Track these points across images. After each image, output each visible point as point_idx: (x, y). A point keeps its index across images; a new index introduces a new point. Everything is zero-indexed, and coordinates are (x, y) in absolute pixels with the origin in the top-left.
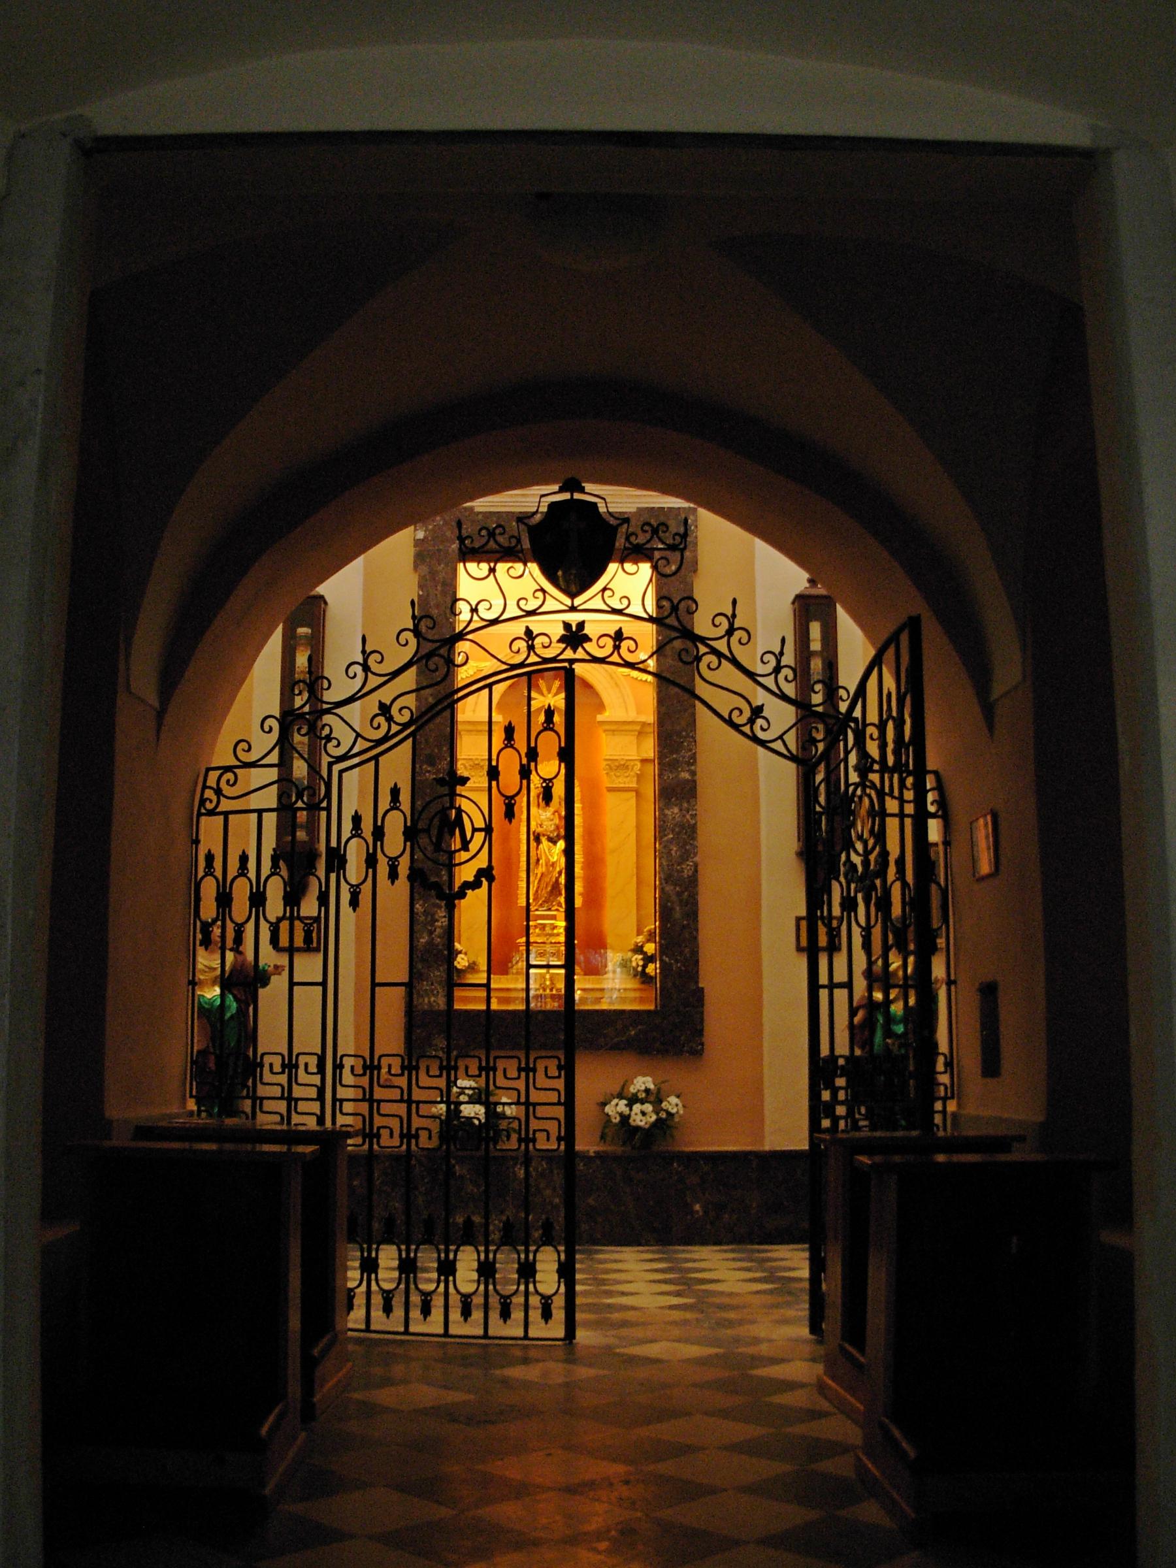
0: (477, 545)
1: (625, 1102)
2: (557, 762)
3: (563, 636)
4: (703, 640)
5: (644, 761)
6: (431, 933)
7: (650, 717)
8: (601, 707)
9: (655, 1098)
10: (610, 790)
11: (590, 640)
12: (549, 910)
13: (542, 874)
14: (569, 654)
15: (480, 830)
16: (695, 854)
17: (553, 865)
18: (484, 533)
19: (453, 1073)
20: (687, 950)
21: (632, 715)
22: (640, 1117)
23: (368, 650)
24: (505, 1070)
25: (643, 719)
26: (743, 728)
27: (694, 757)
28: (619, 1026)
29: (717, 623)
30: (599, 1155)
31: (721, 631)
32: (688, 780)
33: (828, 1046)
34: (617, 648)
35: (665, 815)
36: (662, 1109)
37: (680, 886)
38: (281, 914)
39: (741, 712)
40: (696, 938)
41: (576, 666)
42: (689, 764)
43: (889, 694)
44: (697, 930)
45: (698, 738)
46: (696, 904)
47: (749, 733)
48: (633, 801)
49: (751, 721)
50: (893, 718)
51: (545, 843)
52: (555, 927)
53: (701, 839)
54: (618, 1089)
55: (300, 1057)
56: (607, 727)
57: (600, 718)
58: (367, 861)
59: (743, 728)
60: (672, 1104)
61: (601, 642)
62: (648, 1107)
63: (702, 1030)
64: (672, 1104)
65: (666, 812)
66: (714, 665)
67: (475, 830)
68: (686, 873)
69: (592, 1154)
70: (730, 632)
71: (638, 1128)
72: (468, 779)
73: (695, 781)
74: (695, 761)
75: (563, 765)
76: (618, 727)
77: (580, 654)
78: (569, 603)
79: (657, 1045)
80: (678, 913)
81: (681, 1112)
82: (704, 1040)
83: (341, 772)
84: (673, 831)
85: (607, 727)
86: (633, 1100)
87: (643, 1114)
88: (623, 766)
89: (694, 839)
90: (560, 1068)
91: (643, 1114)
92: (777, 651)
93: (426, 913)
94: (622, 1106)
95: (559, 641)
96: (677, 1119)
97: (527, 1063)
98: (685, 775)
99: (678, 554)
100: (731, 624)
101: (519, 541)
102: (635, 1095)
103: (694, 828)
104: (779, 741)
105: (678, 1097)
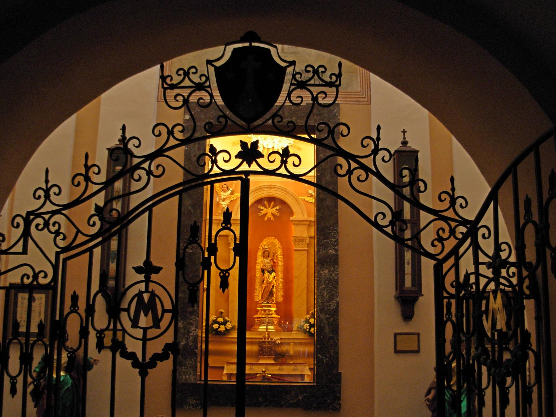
0: (174, 82)
3: (240, 153)
4: (354, 158)
5: (310, 238)
6: (187, 339)
7: (313, 218)
8: (292, 213)
10: (296, 250)
11: (262, 156)
12: (268, 303)
14: (245, 167)
15: (168, 311)
16: (337, 296)
17: (270, 283)
18: (181, 72)
20: (332, 351)
21: (306, 217)
23: (89, 164)
25: (310, 219)
27: (337, 241)
28: (293, 394)
29: (365, 144)
31: (368, 151)
32: (333, 254)
34: (284, 163)
35: (321, 274)
37: (329, 314)
38: (104, 326)
40: (337, 344)
41: (251, 178)
42: (334, 245)
43: (528, 202)
46: (337, 325)
48: (306, 255)
50: (534, 223)
51: (266, 274)
52: (271, 311)
53: (341, 288)
56: (295, 223)
57: (291, 218)
58: (80, 332)
61: (272, 158)
63: (340, 396)
65: (321, 272)
66: (363, 178)
67: (164, 311)
68: (333, 307)
70: (376, 151)
72: (160, 268)
73: (337, 255)
74: (338, 243)
75: (237, 258)
76: (299, 223)
77: (254, 167)
78: (246, 127)
79: (315, 405)
82: (341, 402)
83: (65, 260)
85: (295, 223)
88: (301, 240)
89: (337, 288)
93: (184, 328)
95: (236, 157)
98: (332, 252)
99: (334, 89)
100: (376, 146)
101: (208, 78)
103: (337, 282)
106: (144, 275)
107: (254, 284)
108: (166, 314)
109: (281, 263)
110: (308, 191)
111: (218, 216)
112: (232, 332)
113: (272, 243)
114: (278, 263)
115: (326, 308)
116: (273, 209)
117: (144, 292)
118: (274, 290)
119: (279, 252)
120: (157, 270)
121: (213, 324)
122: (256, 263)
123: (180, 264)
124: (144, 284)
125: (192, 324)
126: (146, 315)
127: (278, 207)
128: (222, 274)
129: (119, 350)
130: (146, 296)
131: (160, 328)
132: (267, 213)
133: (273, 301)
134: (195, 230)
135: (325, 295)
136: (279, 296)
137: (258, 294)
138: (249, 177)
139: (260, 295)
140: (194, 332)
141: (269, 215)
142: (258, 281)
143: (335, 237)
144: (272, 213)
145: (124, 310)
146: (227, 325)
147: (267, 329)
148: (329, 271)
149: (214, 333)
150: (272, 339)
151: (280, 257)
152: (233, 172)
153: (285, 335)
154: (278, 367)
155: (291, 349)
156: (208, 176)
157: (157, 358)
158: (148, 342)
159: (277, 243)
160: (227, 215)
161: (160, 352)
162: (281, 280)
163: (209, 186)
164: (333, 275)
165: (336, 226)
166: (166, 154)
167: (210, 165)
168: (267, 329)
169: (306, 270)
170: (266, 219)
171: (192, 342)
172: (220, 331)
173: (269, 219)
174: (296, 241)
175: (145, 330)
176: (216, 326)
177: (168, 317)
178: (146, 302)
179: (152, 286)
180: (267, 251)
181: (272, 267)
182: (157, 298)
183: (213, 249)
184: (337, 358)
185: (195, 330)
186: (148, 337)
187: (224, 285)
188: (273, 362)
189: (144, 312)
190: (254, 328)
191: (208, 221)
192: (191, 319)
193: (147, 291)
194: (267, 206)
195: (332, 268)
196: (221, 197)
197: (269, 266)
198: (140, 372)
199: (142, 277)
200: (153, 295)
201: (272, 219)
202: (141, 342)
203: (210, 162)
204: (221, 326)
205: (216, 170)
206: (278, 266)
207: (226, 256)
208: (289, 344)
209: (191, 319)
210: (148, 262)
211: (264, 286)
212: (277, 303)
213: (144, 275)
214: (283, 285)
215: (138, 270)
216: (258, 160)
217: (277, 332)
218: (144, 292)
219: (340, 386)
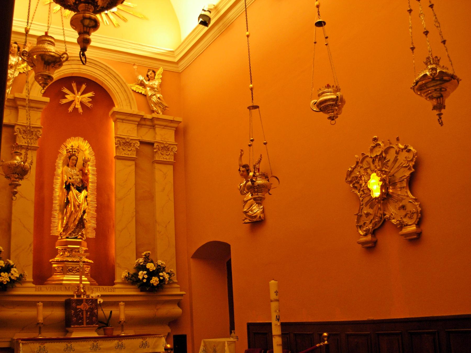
12: (76, 238)
51: (74, 191)
107: (51, 208)
110: (137, 76)
112: (18, 285)
127: (90, 94)
146: (12, 272)
150: (88, 296)
153: (107, 290)
154: (140, 340)
155: (122, 313)
169: (133, 190)
170: (71, 109)
180: (74, 155)
181: (82, 181)
188: (96, 335)
197: (77, 178)
201: (81, 110)
208: (116, 304)
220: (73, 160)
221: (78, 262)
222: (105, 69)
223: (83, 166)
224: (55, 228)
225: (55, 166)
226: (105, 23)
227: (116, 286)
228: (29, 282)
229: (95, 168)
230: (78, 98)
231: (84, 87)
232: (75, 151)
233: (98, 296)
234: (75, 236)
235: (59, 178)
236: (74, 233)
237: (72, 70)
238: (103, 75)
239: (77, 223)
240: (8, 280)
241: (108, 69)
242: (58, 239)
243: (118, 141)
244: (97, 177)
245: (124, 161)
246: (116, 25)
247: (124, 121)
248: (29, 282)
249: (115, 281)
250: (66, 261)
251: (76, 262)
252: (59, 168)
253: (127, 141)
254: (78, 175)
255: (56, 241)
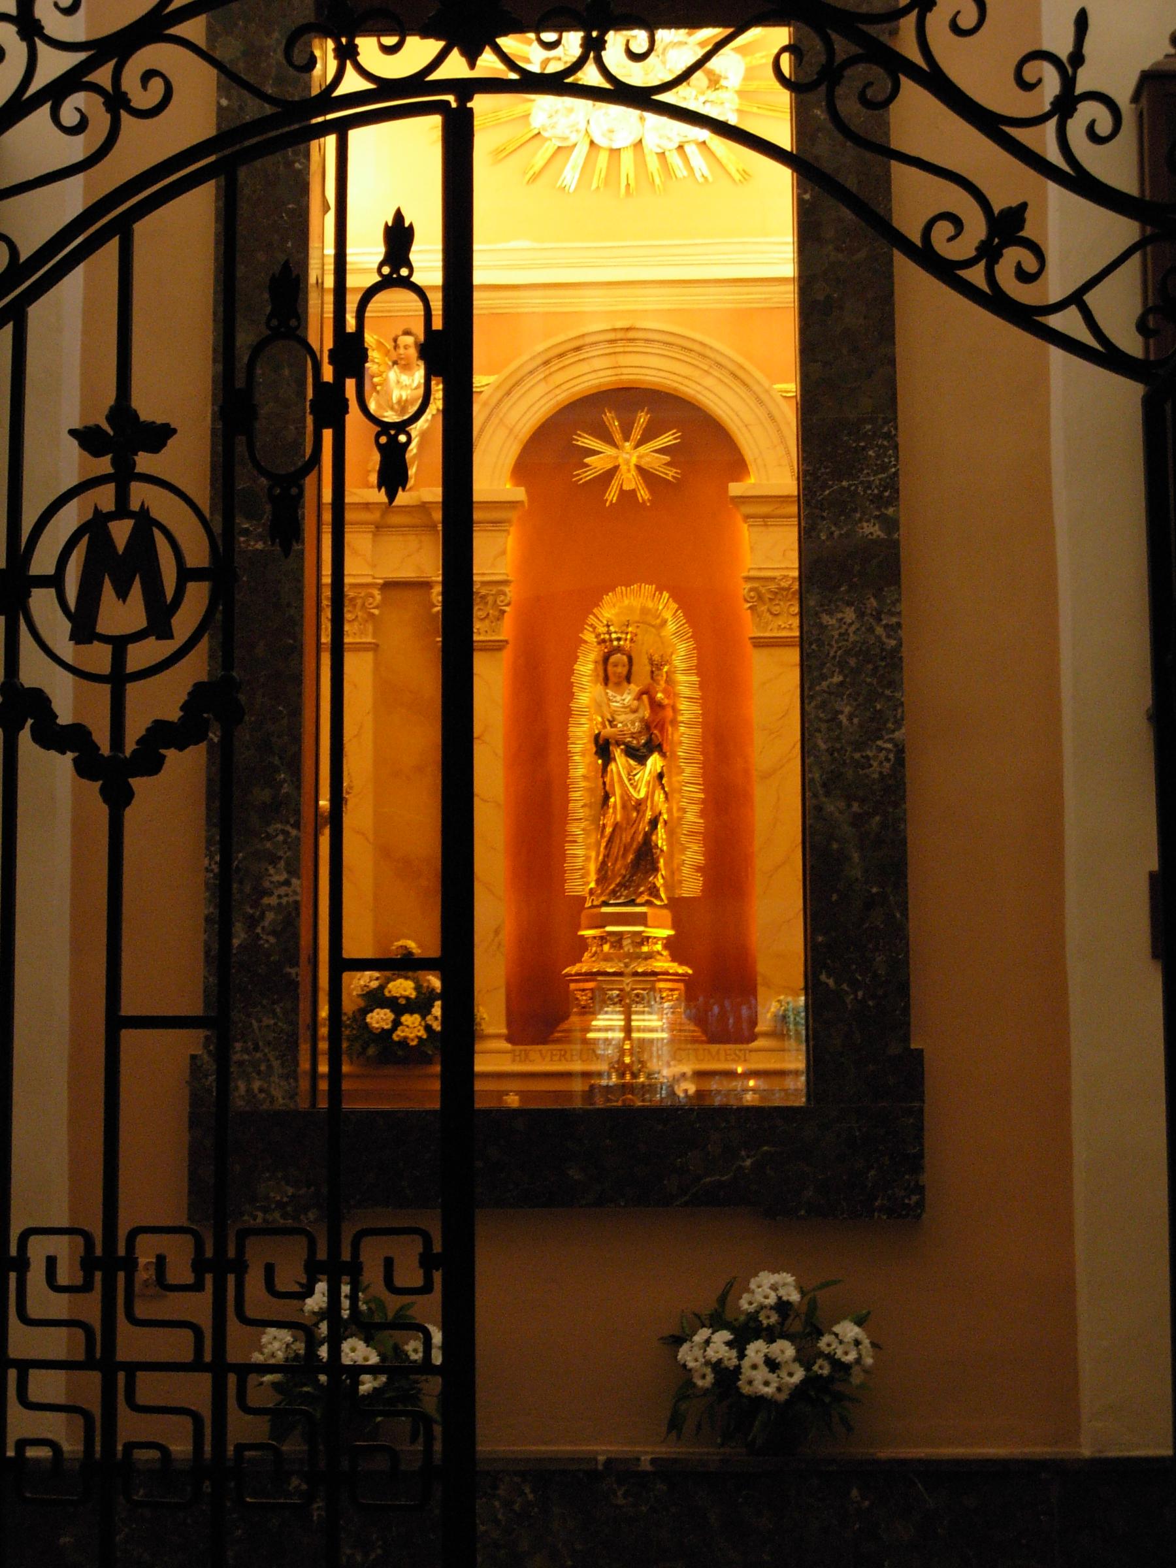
1: (726, 1335)
2: (419, 375)
6: (252, 923)
8: (738, 466)
9: (801, 1324)
10: (760, 643)
12: (632, 903)
13: (616, 826)
14: (455, 67)
16: (899, 724)
17: (639, 805)
19: (231, 1279)
22: (762, 1373)
24: (269, 1270)
26: (965, 274)
30: (664, 1469)
33: (324, 546)
35: (823, 627)
36: (821, 1354)
37: (863, 801)
39: (957, 222)
41: (480, 103)
44: (904, 907)
45: (901, 439)
47: (982, 284)
49: (989, 253)
51: (621, 762)
54: (707, 1305)
55: (142, 1240)
57: (735, 489)
59: (965, 274)
60: (846, 1338)
62: (785, 1350)
63: (921, 1155)
64: (846, 1338)
65: (826, 619)
67: (186, 575)
68: (877, 769)
69: (646, 1466)
70: (1065, 105)
71: (760, 1401)
73: (895, 544)
77: (488, 64)
80: (855, 869)
81: (869, 1361)
82: (925, 1179)
84: (842, 665)
86: (745, 1332)
87: (772, 1365)
89: (894, 685)
90: (427, 1262)
91: (772, 1365)
92: (1063, 50)
94: (719, 1345)
96: (857, 1377)
97: (220, 1247)
98: (871, 529)
100: (1068, 82)
102: (753, 1317)
103: (894, 660)
104: (1073, 311)
105: (859, 1323)
106: (110, 456)
107: (564, 816)
108: (191, 586)
109: (687, 710)
111: (366, 255)
113: (645, 611)
114: (675, 710)
115: (850, 773)
116: (642, 449)
117: (112, 516)
118: (660, 838)
119: (681, 654)
120: (158, 436)
121: (365, 1011)
122: (567, 713)
123: (235, 408)
124: (111, 487)
125: (274, 860)
126: (122, 593)
127: (667, 439)
128: (383, 440)
129: (30, 722)
130: (121, 531)
131: (171, 637)
132: (616, 468)
133: (654, 891)
134: (289, 285)
135: (843, 718)
136: (683, 867)
137: (583, 863)
138: (469, 105)
139: (592, 867)
140: (283, 890)
141: (629, 479)
142: (580, 798)
143: (884, 468)
144: (639, 468)
145: (43, 581)
147: (628, 1029)
148: (861, 615)
149: (371, 1051)
151: (686, 683)
152: (417, 83)
156: (327, 100)
157: (163, 736)
158: (130, 687)
159: (668, 615)
160: (399, 237)
161: (173, 714)
162: (694, 791)
163: (331, 141)
164: (879, 630)
165: (886, 421)
166: (176, 30)
167: (332, 65)
168: (628, 1029)
170: (612, 495)
171: (273, 933)
172: (404, 1042)
173: (628, 496)
174: (760, 597)
175: (119, 644)
176: (380, 1018)
177: (197, 596)
178: (121, 549)
179: (140, 494)
180: (619, 649)
181: (647, 726)
182: (158, 535)
183: (351, 353)
184: (904, 989)
185: (287, 883)
186: (132, 666)
187: (393, 474)
189: (113, 582)
190: (564, 1026)
191: (327, 516)
192: (269, 837)
193: (122, 510)
194: (618, 437)
195: (873, 602)
196: (389, 394)
197: (629, 724)
198: (102, 791)
199: (104, 465)
200: (145, 522)
201: (643, 494)
202: (107, 688)
203: (331, 54)
204: (406, 1019)
205: (352, 83)
206: (675, 723)
207: (397, 383)
209: (269, 837)
210: (122, 411)
211: (609, 821)
212: (677, 905)
213: (110, 456)
214: (703, 814)
215: (88, 438)
216: (501, 41)
217: (679, 1044)
218: (112, 516)
219: (921, 1111)
220: (616, 665)
221: (620, 974)
222: (700, 354)
223: (652, 678)
224: (577, 875)
225: (571, 685)
226: (701, 180)
227: (759, 1043)
228: (497, 1036)
229: (695, 678)
230: (627, 459)
231: (642, 419)
232: (619, 639)
233: (684, 1075)
234: (626, 897)
235: (583, 720)
236: (626, 888)
237: (593, 376)
238: (696, 374)
239: (630, 857)
240: (422, 1033)
241: (708, 353)
242: (583, 908)
243: (751, 590)
244: (703, 706)
245: (773, 651)
246: (737, 177)
247: (770, 521)
248: (497, 1036)
249: (757, 1029)
250: (600, 973)
251: (615, 974)
252: (583, 689)
253: (784, 584)
254: (635, 711)
255: (579, 913)
